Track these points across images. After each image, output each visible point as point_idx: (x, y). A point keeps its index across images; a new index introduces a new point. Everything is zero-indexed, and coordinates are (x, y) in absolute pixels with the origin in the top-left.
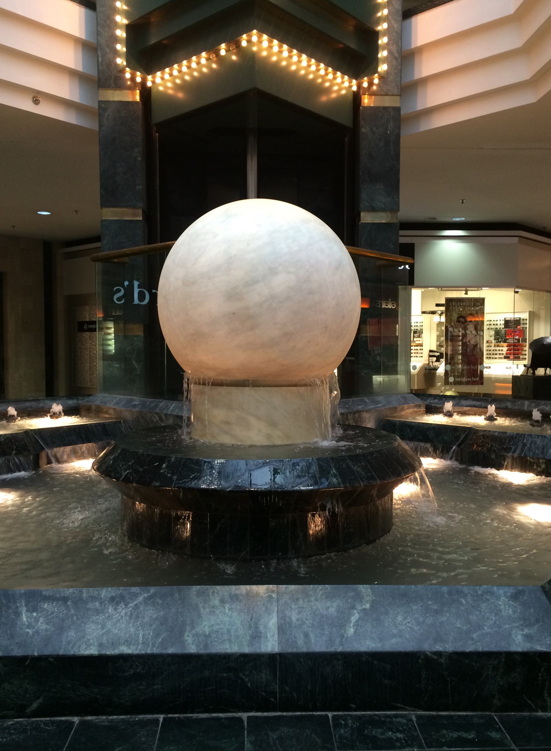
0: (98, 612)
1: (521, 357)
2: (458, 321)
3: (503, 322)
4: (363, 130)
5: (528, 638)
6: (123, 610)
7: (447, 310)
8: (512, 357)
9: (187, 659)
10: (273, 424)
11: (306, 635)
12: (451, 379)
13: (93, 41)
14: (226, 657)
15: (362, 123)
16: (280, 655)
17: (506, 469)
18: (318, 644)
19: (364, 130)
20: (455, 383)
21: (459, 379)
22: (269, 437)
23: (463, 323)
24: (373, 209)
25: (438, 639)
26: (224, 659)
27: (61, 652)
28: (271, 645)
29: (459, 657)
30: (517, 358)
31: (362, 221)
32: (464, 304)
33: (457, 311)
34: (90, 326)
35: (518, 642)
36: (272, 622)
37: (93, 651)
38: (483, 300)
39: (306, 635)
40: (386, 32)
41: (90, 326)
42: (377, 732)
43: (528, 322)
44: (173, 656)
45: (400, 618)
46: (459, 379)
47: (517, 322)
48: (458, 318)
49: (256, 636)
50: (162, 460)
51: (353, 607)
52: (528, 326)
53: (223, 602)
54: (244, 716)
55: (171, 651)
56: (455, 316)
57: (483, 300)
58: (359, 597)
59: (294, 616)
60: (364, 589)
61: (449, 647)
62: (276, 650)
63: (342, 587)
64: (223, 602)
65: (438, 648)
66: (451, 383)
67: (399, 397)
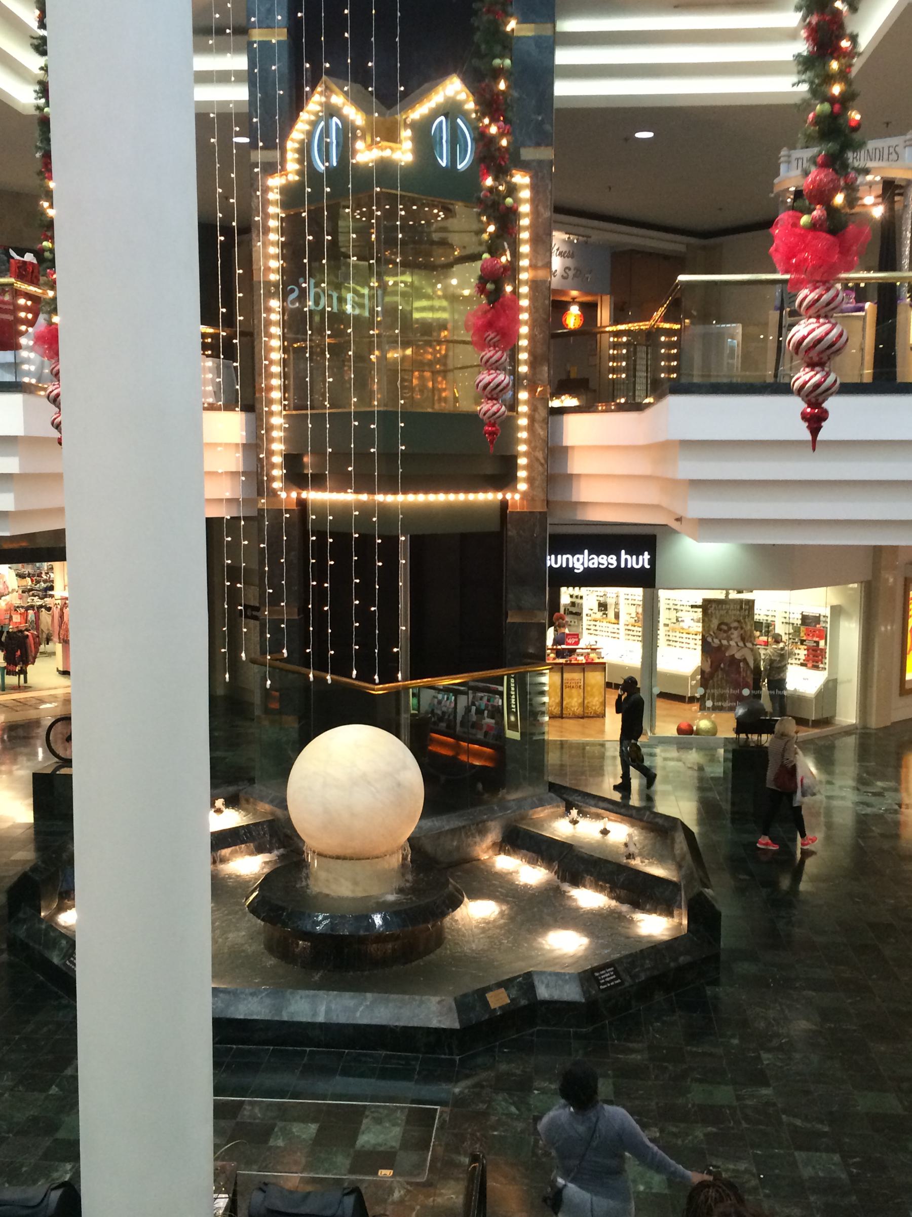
0: (244, 999)
1: (821, 666)
2: (719, 629)
3: (800, 617)
4: (510, 533)
5: (440, 1021)
6: (255, 999)
7: (705, 613)
8: (810, 665)
9: (284, 1022)
10: (356, 883)
11: (337, 1016)
12: (709, 704)
13: (254, 442)
14: (300, 1023)
15: (509, 526)
16: (324, 1023)
17: (585, 886)
18: (342, 1019)
19: (512, 532)
20: (714, 709)
21: (720, 704)
22: (353, 891)
23: (725, 632)
24: (520, 609)
25: (398, 1019)
26: (300, 1024)
27: (228, 1016)
28: (321, 1019)
29: (405, 1029)
30: (816, 667)
31: (509, 620)
32: (728, 606)
33: (718, 616)
34: (255, 613)
35: (434, 1023)
36: (322, 1009)
37: (242, 1017)
38: (753, 601)
39: (337, 1016)
40: (526, 454)
41: (255, 613)
42: (363, 1059)
43: (829, 620)
44: (277, 1021)
45: (382, 1010)
46: (720, 704)
47: (817, 619)
48: (720, 625)
49: (315, 1014)
50: (283, 909)
51: (361, 1004)
52: (828, 626)
53: (301, 998)
54: (308, 1049)
55: (277, 1018)
56: (715, 623)
57: (753, 601)
58: (365, 999)
59: (333, 1006)
60: (369, 995)
61: (402, 1023)
62: (323, 1021)
63: (357, 994)
64: (301, 998)
65: (397, 1024)
66: (709, 708)
67: (534, 799)
